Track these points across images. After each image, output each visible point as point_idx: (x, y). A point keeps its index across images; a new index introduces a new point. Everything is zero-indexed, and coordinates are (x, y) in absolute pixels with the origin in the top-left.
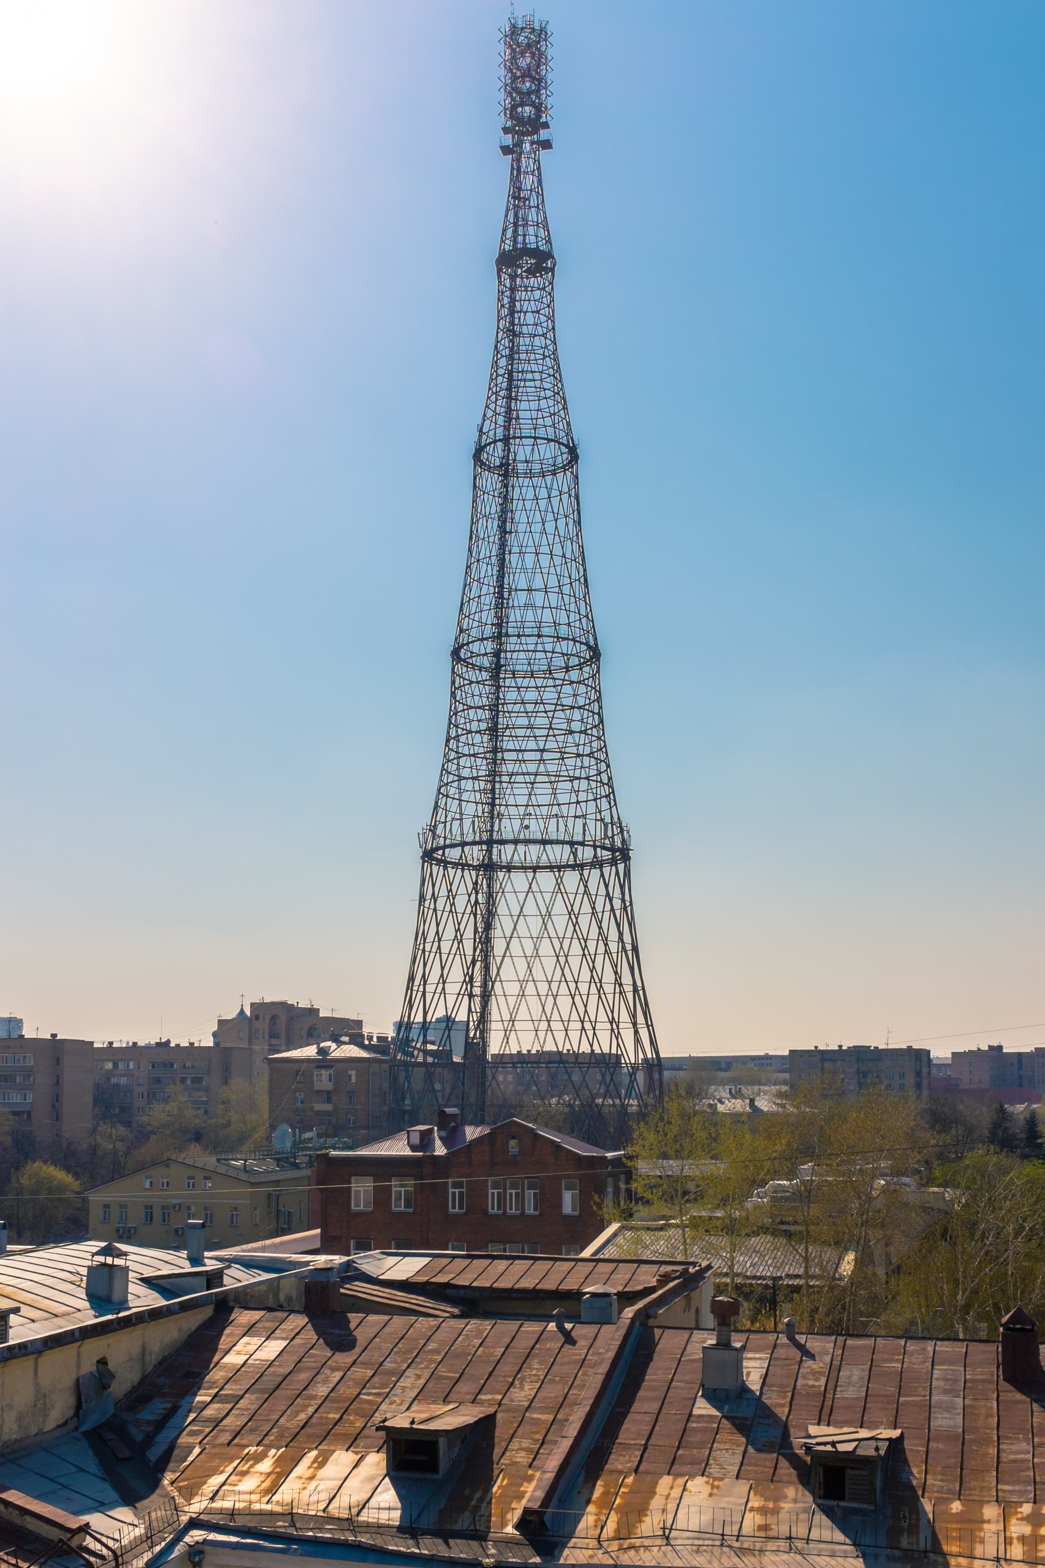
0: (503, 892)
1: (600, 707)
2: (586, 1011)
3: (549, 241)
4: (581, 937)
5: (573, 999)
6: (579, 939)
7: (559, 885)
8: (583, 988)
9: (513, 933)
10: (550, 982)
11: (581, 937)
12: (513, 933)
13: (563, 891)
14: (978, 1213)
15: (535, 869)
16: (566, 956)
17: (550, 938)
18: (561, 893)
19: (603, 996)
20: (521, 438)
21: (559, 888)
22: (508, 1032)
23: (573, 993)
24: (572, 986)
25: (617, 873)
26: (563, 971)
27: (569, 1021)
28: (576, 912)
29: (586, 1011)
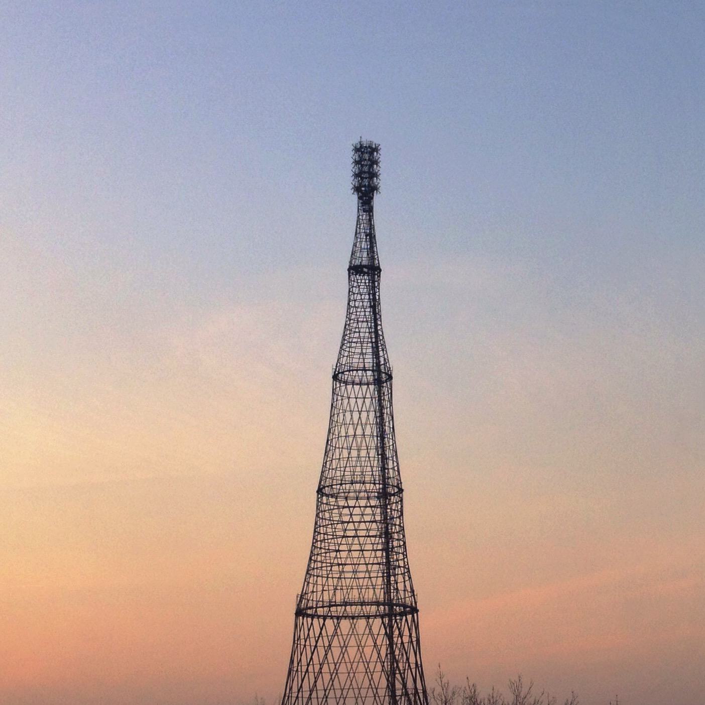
0: (337, 673)
1: (404, 536)
3: (416, 603)
4: (365, 661)
5: (356, 700)
7: (353, 630)
8: (363, 692)
9: (339, 700)
10: (342, 690)
12: (339, 700)
13: (355, 633)
15: (338, 618)
16: (354, 673)
19: (377, 698)
22: (327, 691)
23: (357, 696)
24: (357, 691)
25: (406, 620)
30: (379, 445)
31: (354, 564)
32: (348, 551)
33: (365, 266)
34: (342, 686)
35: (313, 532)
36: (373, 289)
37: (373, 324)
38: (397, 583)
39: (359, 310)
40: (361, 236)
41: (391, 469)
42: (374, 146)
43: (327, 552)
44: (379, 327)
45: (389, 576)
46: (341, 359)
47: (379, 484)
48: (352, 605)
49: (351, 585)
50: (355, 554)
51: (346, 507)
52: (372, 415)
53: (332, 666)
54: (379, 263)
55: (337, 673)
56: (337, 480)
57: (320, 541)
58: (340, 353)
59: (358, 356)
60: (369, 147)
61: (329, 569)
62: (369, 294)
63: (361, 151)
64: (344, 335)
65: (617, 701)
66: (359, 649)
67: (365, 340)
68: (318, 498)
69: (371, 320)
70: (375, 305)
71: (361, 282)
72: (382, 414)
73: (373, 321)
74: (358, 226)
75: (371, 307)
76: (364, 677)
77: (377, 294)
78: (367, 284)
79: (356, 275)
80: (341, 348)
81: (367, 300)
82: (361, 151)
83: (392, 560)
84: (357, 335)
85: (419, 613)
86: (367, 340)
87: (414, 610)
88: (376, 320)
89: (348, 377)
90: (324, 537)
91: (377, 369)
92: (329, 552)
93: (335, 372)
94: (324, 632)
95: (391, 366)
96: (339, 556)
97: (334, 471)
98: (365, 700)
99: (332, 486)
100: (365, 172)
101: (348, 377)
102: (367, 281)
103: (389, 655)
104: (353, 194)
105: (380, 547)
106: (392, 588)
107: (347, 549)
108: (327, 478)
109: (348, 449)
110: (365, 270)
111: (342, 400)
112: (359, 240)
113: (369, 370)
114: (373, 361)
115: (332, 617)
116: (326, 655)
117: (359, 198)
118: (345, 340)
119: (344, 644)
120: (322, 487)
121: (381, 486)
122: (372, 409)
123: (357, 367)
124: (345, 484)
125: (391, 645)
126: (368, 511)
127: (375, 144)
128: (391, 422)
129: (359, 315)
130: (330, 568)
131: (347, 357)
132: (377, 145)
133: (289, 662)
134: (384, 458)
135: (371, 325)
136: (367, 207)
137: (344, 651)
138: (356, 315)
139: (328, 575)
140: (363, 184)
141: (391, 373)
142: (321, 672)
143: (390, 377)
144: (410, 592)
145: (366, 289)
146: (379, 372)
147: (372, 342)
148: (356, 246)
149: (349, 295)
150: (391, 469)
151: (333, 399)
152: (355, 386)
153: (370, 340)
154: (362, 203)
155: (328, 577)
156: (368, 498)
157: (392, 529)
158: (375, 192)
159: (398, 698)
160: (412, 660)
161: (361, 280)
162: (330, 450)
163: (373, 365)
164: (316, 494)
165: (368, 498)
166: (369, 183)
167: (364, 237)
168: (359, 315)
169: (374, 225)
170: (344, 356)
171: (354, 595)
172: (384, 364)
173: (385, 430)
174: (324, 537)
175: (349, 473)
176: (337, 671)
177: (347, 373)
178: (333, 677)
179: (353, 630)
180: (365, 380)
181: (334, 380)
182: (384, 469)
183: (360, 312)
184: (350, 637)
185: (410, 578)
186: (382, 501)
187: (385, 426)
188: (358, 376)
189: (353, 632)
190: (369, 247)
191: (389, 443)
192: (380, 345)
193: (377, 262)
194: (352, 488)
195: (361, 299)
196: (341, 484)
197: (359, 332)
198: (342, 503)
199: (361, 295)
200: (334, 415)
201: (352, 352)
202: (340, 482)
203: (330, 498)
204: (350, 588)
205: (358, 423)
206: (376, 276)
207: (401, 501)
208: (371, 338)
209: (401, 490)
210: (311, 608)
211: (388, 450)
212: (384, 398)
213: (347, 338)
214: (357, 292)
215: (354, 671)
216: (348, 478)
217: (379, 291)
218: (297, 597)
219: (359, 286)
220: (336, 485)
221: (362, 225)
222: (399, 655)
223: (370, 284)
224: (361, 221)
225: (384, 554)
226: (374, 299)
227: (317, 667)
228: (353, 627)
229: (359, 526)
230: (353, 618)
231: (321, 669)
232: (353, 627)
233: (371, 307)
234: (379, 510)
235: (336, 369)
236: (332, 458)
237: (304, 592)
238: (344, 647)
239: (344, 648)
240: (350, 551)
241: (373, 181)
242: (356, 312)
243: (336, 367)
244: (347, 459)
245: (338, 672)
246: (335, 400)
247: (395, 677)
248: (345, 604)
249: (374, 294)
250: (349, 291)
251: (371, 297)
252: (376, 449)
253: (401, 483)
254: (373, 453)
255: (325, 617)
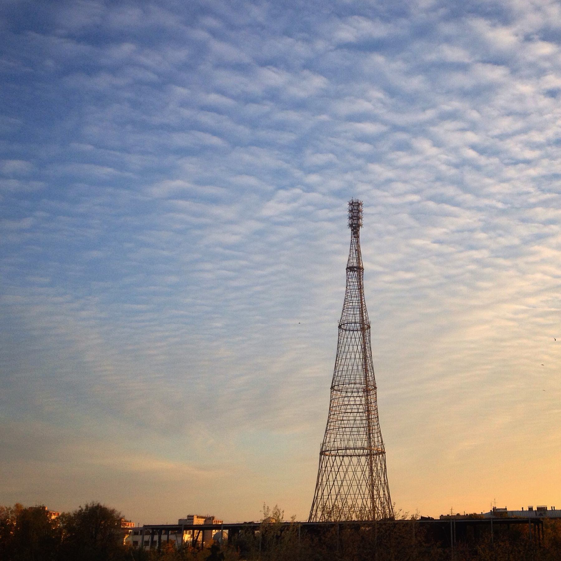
0: (351, 486)
2: (367, 504)
6: (362, 465)
7: (359, 463)
10: (355, 495)
11: (361, 466)
13: (361, 464)
14: (11, 347)
16: (361, 486)
17: (356, 480)
18: (360, 465)
20: (359, 384)
21: (359, 464)
23: (363, 498)
24: (362, 496)
26: (360, 491)
27: (363, 480)
28: (365, 470)
29: (367, 504)
30: (364, 363)
31: (358, 427)
32: (356, 420)
33: (355, 267)
34: (364, 493)
35: (329, 410)
36: (360, 279)
37: (360, 299)
38: (374, 438)
39: (352, 291)
40: (353, 251)
41: (370, 376)
42: (359, 202)
43: (336, 421)
44: (363, 300)
45: (370, 434)
46: (343, 317)
47: (364, 384)
48: (358, 449)
49: (357, 438)
50: (358, 422)
51: (361, 397)
52: (359, 347)
53: (349, 482)
54: (363, 266)
55: (351, 486)
56: (341, 382)
57: (333, 415)
58: (342, 314)
59: (352, 316)
60: (357, 203)
61: (337, 430)
62: (358, 282)
63: (353, 205)
64: (344, 304)
65: (495, 502)
66: (362, 473)
67: (355, 307)
68: (331, 392)
69: (359, 296)
70: (361, 288)
71: (353, 276)
72: (365, 346)
73: (360, 297)
74: (352, 246)
75: (358, 289)
76: (357, 489)
77: (362, 282)
78: (356, 277)
79: (350, 272)
80: (343, 311)
81: (356, 286)
82: (353, 205)
83: (371, 425)
84: (351, 304)
85: (386, 454)
86: (357, 307)
87: (383, 453)
88: (361, 296)
89: (347, 327)
90: (335, 413)
91: (362, 322)
92: (338, 421)
93: (340, 324)
94: (343, 463)
95: (370, 321)
96: (349, 423)
97: (339, 378)
98: (367, 500)
99: (338, 385)
100: (355, 217)
101: (347, 327)
102: (357, 275)
103: (370, 476)
104: (349, 228)
105: (364, 418)
106: (371, 440)
107: (357, 421)
108: (336, 381)
109: (347, 365)
110: (355, 269)
111: (343, 339)
112: (352, 253)
113: (358, 323)
114: (360, 318)
115: (339, 456)
116: (345, 476)
117: (352, 230)
118: (345, 307)
119: (355, 470)
120: (333, 386)
121: (365, 385)
122: (359, 344)
123: (351, 322)
124: (346, 384)
125: (371, 470)
126: (358, 399)
127: (360, 201)
128: (370, 351)
129: (352, 294)
130: (338, 429)
131: (346, 316)
132: (361, 202)
133: (317, 479)
134: (366, 371)
135: (359, 299)
136: (356, 235)
137: (355, 474)
138: (351, 294)
139: (343, 433)
140: (354, 223)
141: (369, 324)
142: (342, 485)
143: (369, 327)
144: (381, 443)
145: (356, 280)
146: (364, 324)
147: (359, 308)
148: (350, 256)
149: (347, 283)
150: (370, 376)
151: (339, 338)
152: (354, 332)
153: (358, 307)
154: (353, 233)
155: (343, 435)
156: (358, 392)
157: (371, 409)
158: (360, 227)
159: (375, 499)
160: (382, 479)
161: (353, 274)
162: (337, 366)
163: (360, 321)
164: (330, 390)
165: (358, 392)
166: (357, 222)
167: (354, 251)
168: (352, 294)
169: (360, 245)
170: (344, 316)
171: (351, 444)
172: (366, 320)
173: (367, 355)
174: (335, 413)
175: (347, 379)
176: (351, 485)
177: (346, 325)
178: (349, 488)
179: (359, 463)
180: (355, 328)
181: (339, 329)
182: (366, 377)
183: (353, 292)
184: (358, 467)
185: (381, 435)
186: (365, 394)
187: (367, 353)
188: (352, 326)
189: (359, 464)
190: (357, 257)
191: (369, 362)
192: (363, 309)
193: (362, 265)
194: (355, 387)
195: (353, 285)
196: (343, 384)
197: (353, 303)
198: (344, 394)
199: (353, 283)
200: (339, 347)
201: (349, 314)
202: (342, 383)
203: (338, 392)
204: (356, 440)
205: (356, 352)
206: (361, 273)
207: (376, 393)
208: (359, 306)
209: (375, 388)
210: (328, 451)
211: (368, 366)
212: (366, 338)
213: (346, 306)
214: (351, 281)
215: (361, 484)
216: (347, 381)
217: (363, 281)
218: (321, 445)
219: (352, 278)
220: (341, 385)
221: (354, 245)
222: (376, 476)
223: (358, 277)
224: (353, 242)
225: (367, 422)
226: (360, 284)
227: (340, 483)
228: (359, 461)
229: (359, 407)
230: (359, 456)
231: (342, 483)
232: (359, 461)
233: (358, 289)
234: (363, 399)
235: (340, 323)
236: (339, 370)
237: (324, 442)
238: (355, 472)
239: (355, 472)
240: (355, 420)
241: (359, 221)
242: (351, 292)
243: (340, 321)
244: (346, 371)
245: (352, 485)
246: (340, 339)
247: (373, 488)
248: (346, 449)
249: (360, 282)
250: (347, 281)
251: (359, 284)
252: (362, 366)
253: (376, 384)
254: (360, 368)
255: (343, 456)
